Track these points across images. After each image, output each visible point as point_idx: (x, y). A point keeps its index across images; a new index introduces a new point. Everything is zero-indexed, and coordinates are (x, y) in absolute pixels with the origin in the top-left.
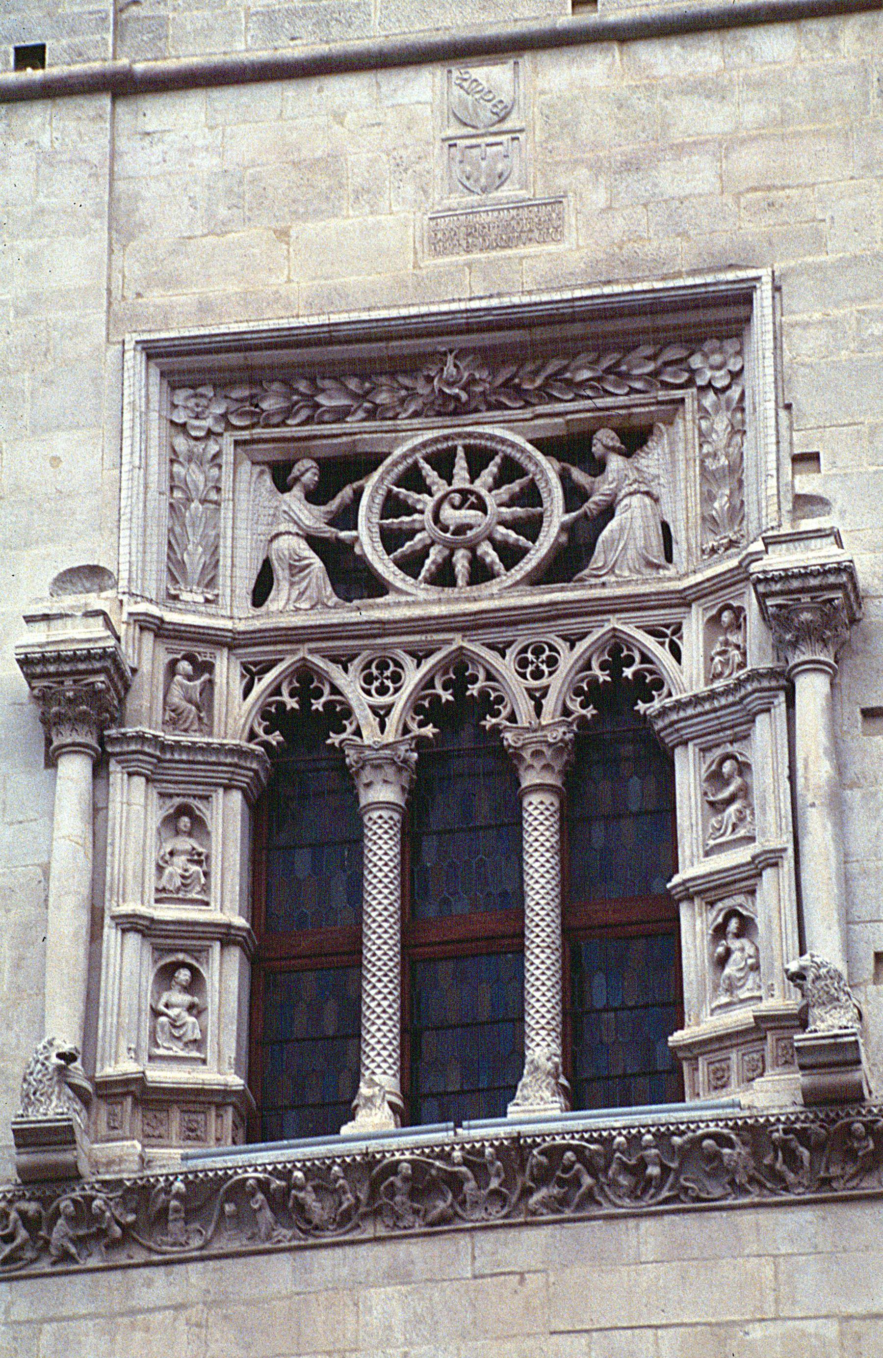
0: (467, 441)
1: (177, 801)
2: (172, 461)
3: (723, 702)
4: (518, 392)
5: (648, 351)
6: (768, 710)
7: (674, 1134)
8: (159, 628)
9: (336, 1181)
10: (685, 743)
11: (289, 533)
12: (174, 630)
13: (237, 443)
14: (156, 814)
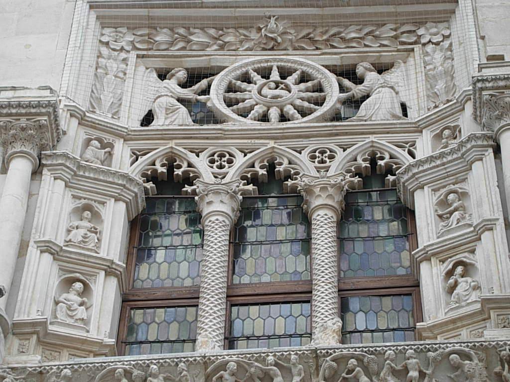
0: (279, 64)
1: (83, 201)
2: (98, 57)
3: (450, 158)
4: (313, 41)
5: (393, 26)
6: (481, 159)
7: (429, 350)
8: (82, 119)
9: (181, 373)
10: (422, 187)
11: (167, 95)
12: (91, 122)
13: (138, 56)
14: (70, 205)
